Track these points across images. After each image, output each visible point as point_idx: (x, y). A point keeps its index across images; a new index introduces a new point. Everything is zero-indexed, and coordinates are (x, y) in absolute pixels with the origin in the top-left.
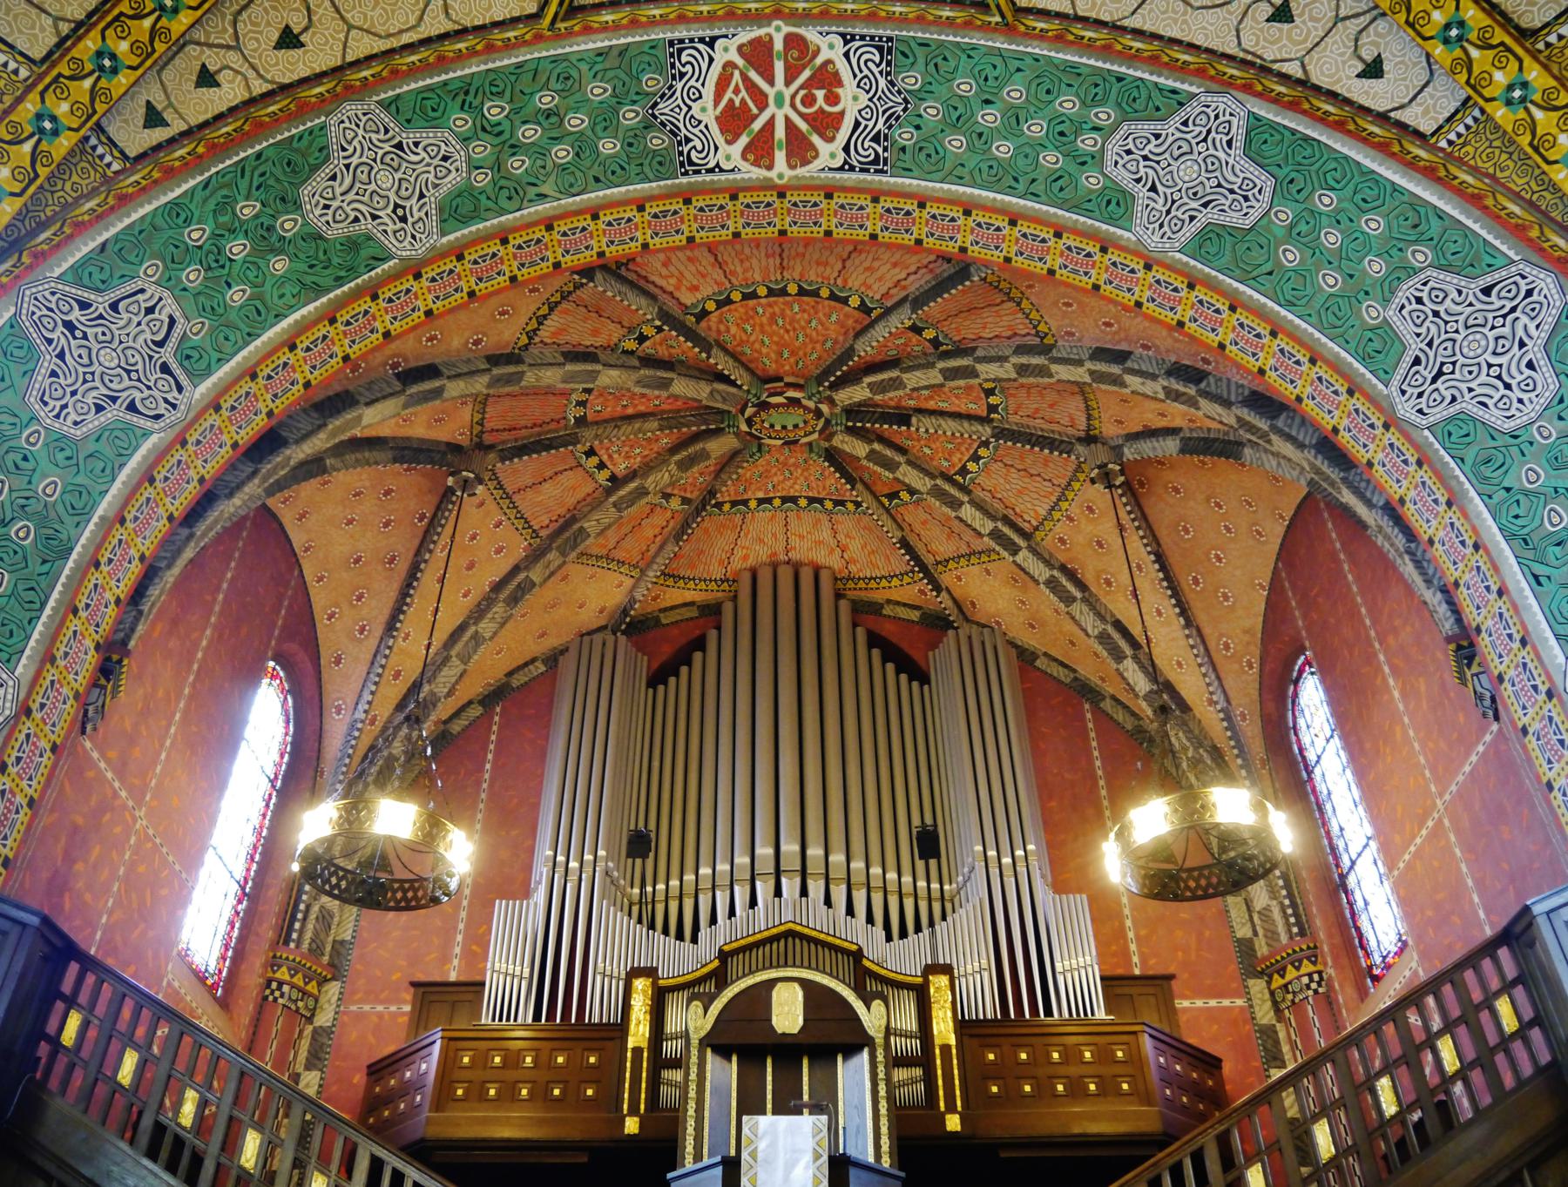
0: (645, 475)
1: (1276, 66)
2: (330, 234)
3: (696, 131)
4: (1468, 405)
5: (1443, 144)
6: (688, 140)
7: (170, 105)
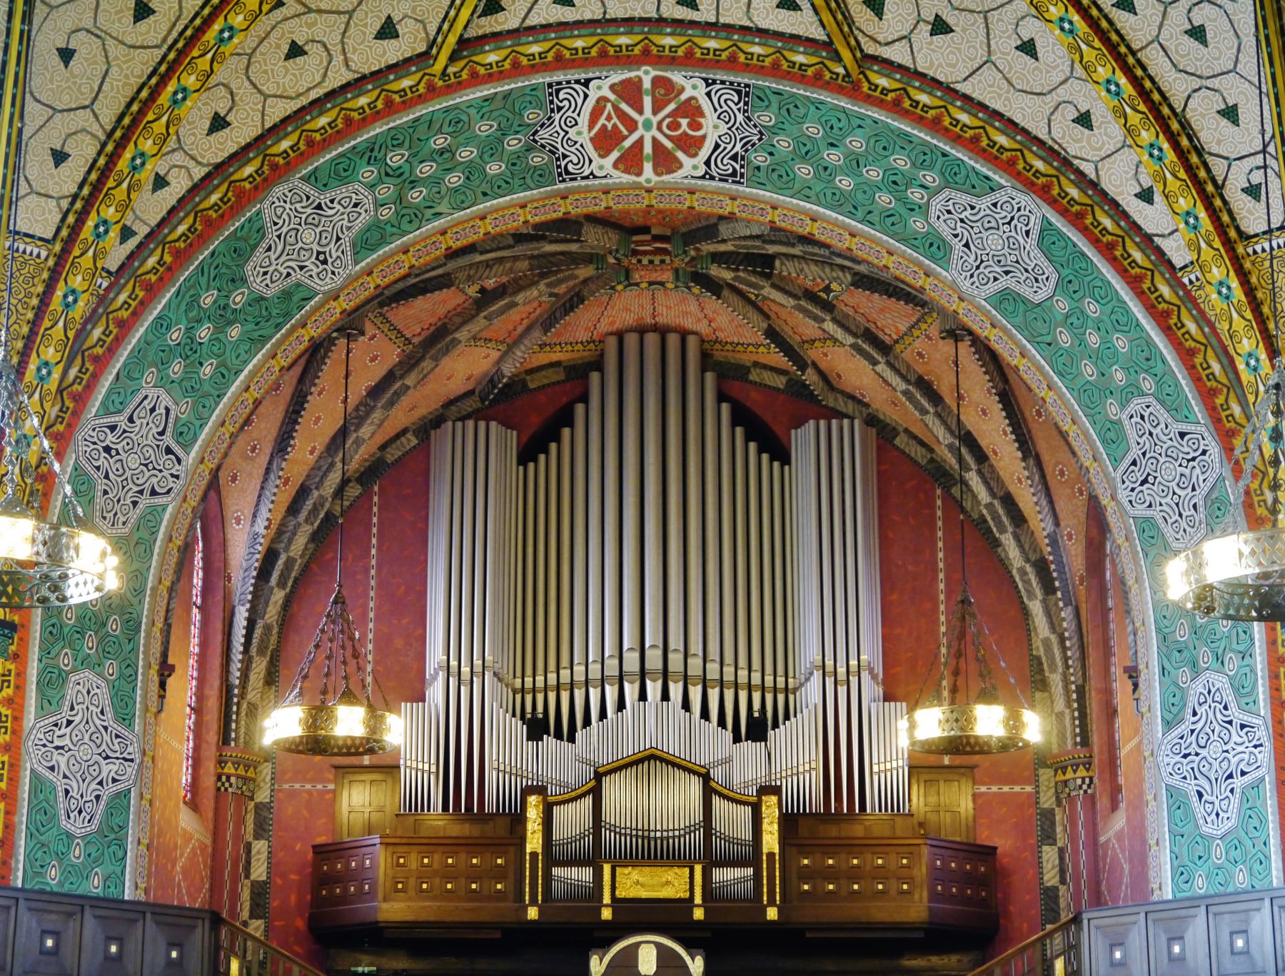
0: (515, 293)
1: (1076, 162)
2: (269, 293)
3: (572, 149)
4: (1155, 513)
5: (1186, 280)
6: (565, 156)
7: (137, 217)
